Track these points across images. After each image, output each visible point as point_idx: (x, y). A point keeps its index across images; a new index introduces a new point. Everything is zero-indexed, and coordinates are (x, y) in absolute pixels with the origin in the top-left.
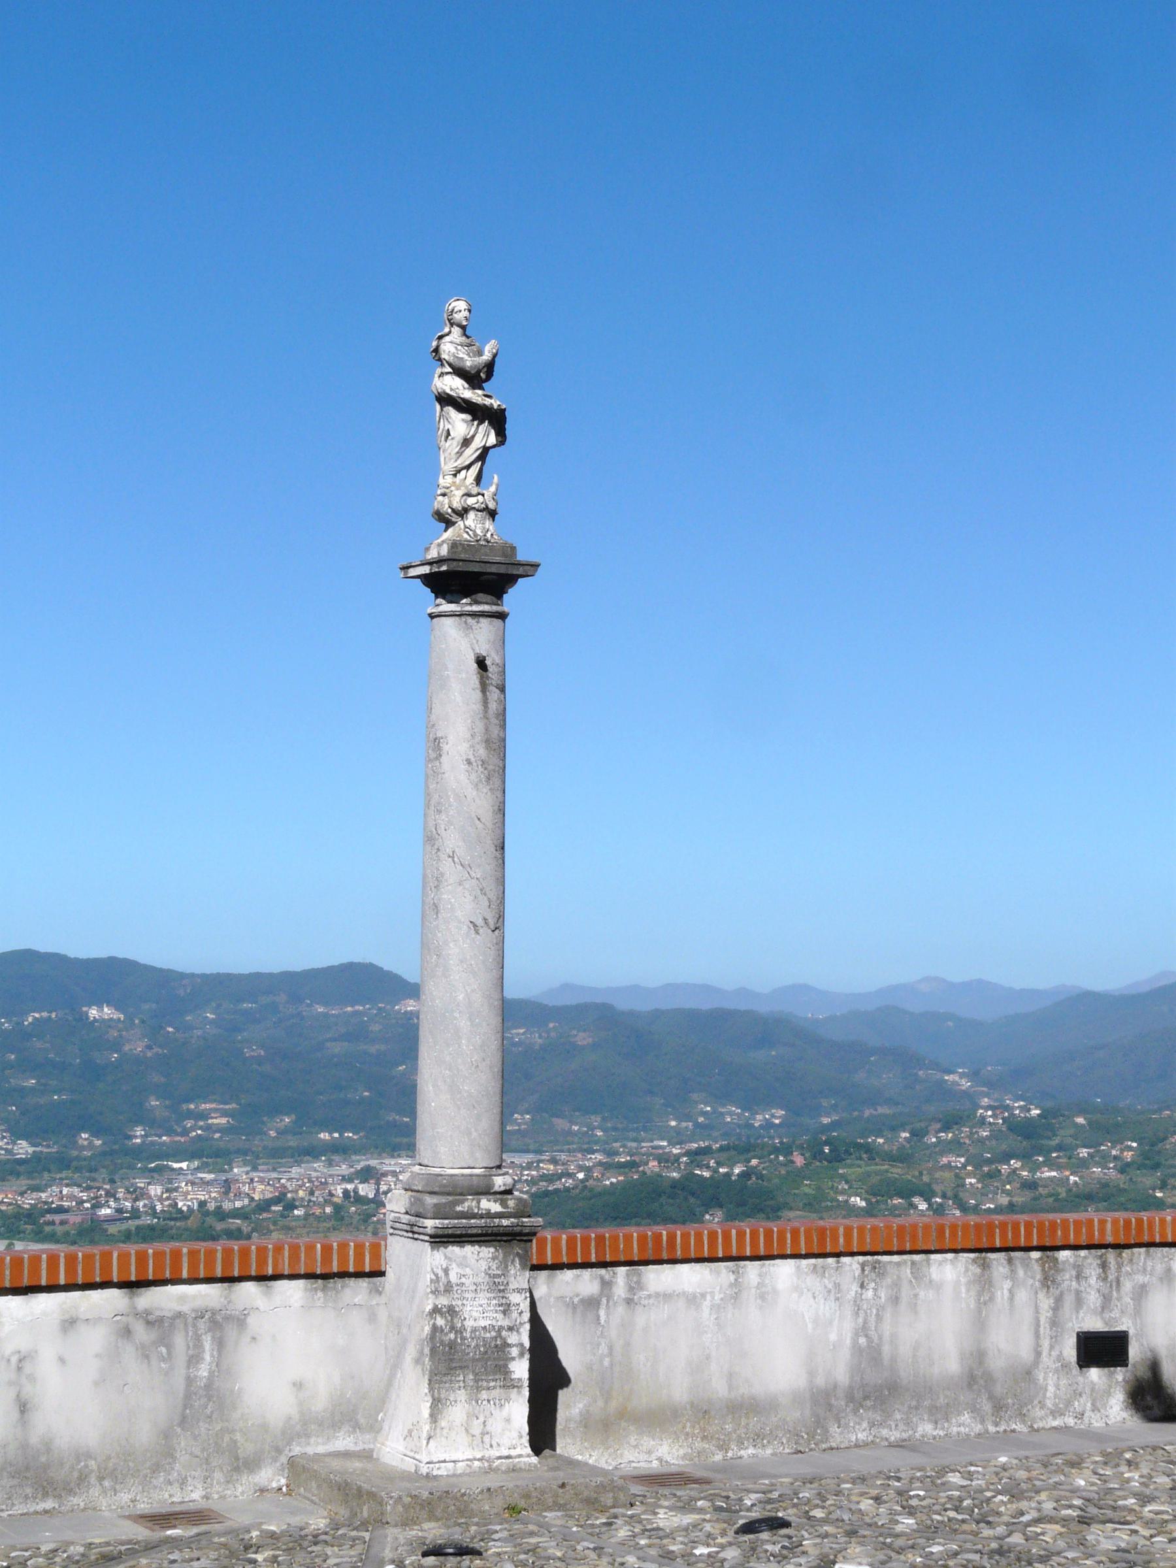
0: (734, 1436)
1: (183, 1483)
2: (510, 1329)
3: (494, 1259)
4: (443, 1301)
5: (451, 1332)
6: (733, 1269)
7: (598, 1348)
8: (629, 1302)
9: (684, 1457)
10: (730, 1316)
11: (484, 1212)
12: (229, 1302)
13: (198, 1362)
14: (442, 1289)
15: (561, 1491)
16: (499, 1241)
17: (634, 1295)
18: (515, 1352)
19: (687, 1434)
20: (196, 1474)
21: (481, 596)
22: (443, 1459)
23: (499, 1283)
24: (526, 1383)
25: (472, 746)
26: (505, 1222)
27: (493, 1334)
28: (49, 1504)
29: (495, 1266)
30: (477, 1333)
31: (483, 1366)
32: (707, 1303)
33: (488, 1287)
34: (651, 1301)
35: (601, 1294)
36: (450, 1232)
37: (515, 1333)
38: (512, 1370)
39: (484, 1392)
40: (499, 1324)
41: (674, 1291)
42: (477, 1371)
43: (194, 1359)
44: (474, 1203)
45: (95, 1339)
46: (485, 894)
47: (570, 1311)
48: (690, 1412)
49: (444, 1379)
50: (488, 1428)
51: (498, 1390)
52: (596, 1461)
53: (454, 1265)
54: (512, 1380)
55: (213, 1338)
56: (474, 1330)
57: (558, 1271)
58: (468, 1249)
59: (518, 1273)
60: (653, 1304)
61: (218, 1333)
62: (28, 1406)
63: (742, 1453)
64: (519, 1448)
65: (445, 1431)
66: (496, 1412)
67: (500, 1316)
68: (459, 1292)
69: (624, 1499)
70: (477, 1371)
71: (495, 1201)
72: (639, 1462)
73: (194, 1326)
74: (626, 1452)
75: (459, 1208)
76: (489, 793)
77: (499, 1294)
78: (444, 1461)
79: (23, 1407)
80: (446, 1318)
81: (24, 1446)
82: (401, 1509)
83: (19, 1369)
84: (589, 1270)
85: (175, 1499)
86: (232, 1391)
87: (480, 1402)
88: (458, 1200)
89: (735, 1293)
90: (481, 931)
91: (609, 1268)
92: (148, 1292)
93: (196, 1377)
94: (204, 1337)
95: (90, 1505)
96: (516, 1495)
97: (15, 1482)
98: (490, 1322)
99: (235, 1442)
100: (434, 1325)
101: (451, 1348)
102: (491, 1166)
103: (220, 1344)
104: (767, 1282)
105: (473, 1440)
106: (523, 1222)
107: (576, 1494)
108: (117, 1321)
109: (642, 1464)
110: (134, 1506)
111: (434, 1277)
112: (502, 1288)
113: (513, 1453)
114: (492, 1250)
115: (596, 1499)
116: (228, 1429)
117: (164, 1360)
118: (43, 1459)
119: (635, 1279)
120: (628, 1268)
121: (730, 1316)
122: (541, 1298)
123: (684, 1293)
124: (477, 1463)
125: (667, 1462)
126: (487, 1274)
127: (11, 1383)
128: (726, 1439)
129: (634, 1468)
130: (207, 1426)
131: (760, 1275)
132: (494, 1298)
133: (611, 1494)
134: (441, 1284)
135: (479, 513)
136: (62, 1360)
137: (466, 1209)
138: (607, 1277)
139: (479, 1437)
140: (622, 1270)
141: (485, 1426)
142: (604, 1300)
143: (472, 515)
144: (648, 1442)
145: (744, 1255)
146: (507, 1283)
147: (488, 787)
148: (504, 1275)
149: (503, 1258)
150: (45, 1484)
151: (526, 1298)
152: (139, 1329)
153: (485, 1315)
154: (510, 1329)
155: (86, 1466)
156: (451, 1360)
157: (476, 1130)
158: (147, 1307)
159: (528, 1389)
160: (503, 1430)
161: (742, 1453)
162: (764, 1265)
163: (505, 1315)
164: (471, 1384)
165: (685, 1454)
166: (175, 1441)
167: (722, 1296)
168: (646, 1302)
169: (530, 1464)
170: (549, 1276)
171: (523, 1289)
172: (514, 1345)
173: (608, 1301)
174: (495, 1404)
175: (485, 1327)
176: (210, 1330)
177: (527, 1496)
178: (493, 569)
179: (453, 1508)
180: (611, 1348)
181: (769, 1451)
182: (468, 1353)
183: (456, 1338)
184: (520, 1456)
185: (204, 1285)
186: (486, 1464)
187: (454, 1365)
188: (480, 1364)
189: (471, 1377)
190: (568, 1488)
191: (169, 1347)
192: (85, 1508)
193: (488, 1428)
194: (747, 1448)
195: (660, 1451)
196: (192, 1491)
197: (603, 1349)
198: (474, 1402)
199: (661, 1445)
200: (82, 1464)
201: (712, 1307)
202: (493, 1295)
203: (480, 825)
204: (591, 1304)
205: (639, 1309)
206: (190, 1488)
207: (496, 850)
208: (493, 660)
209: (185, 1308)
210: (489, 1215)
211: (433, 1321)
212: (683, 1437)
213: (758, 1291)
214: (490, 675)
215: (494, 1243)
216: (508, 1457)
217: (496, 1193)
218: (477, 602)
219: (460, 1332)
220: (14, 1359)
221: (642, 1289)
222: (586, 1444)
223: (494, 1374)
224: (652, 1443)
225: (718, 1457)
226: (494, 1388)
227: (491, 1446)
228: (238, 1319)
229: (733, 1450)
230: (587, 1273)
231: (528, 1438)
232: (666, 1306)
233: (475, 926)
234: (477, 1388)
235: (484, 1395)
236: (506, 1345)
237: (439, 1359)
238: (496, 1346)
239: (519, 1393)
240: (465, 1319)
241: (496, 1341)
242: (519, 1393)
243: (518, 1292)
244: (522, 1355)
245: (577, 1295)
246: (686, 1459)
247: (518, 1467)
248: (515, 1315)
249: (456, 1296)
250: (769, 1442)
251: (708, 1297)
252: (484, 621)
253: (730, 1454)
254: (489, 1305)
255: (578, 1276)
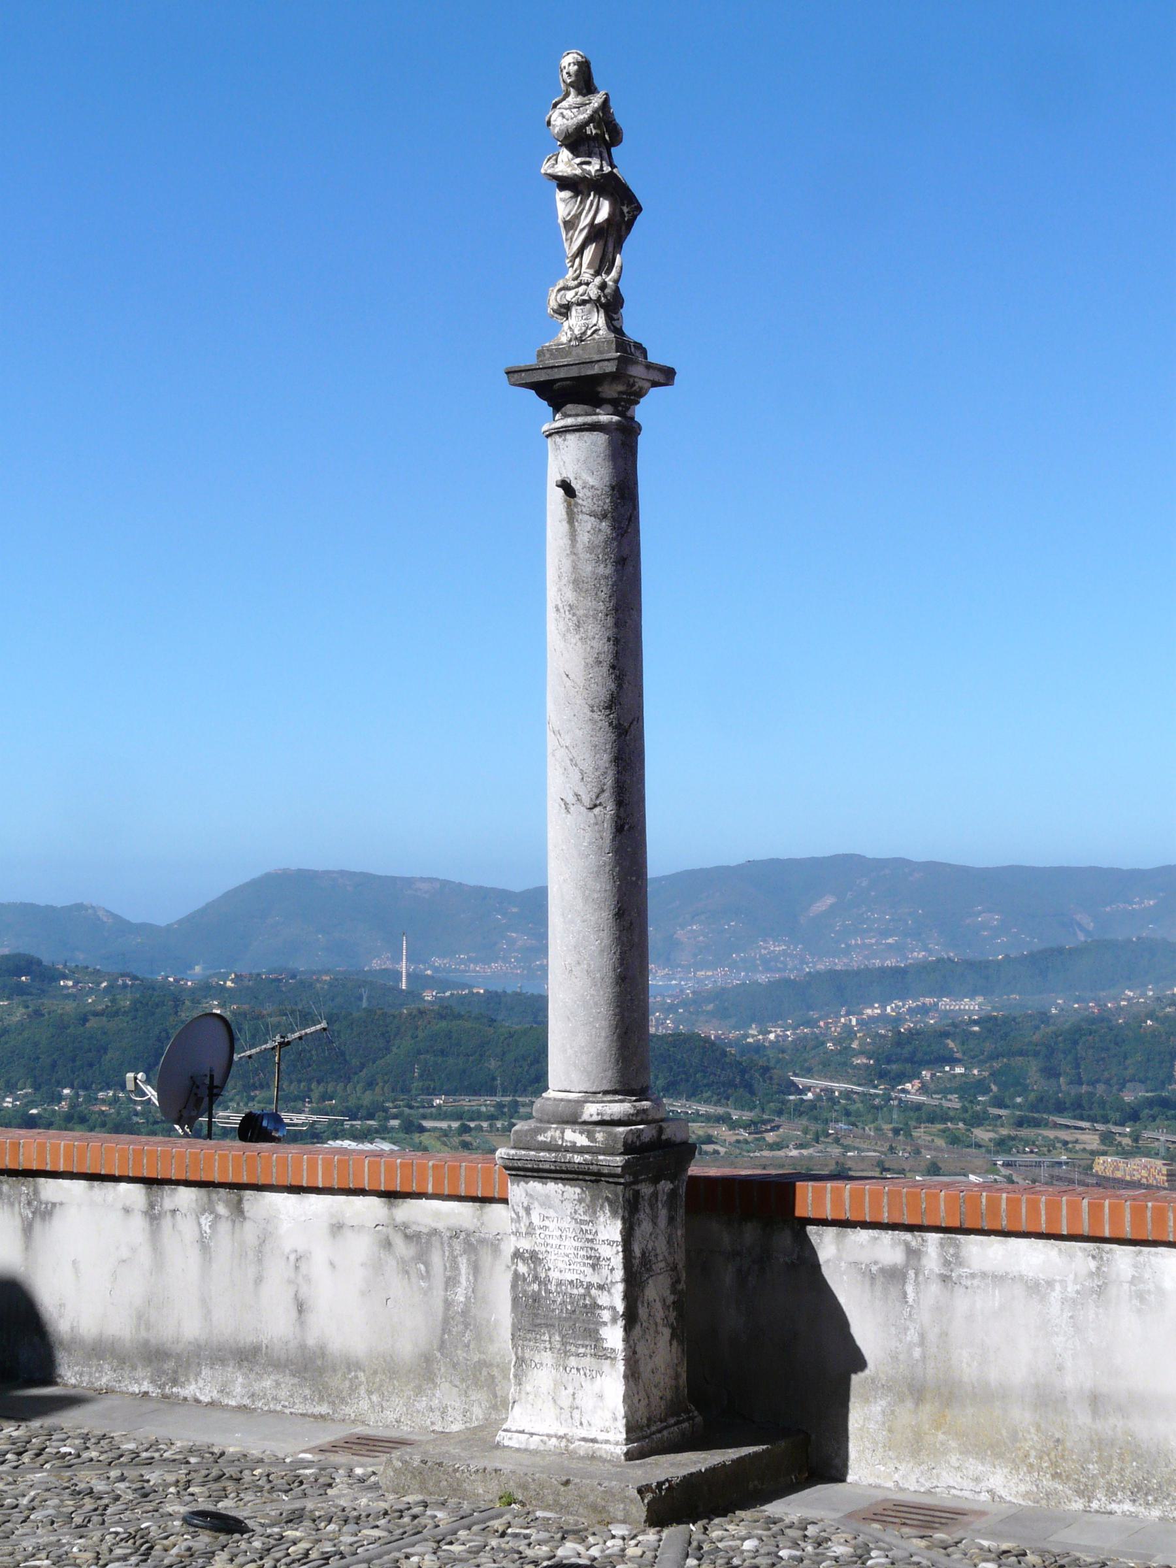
0: (1102, 1482)
1: (443, 1413)
2: (601, 1287)
3: (580, 1201)
4: (525, 1244)
5: (534, 1282)
6: (1094, 1253)
7: (906, 1334)
8: (945, 1279)
9: (1027, 1495)
10: (1091, 1315)
11: (569, 1144)
12: (482, 1224)
13: (454, 1286)
14: (523, 1230)
15: (563, 1488)
16: (585, 1180)
17: (951, 1271)
18: (606, 1315)
19: (1031, 1465)
20: (457, 1405)
21: (569, 408)
22: (521, 1429)
23: (586, 1230)
24: (621, 1355)
25: (560, 590)
26: (578, 1159)
27: (582, 1291)
28: (324, 1409)
29: (582, 1210)
30: (563, 1287)
31: (570, 1327)
32: (1056, 1294)
33: (574, 1234)
34: (976, 1282)
35: (907, 1265)
36: (520, 1164)
37: (606, 1293)
38: (603, 1336)
39: (572, 1358)
40: (588, 1279)
41: (1007, 1273)
42: (564, 1332)
43: (451, 1282)
44: (558, 1134)
45: (360, 1247)
46: (576, 765)
47: (867, 1280)
48: (1036, 1438)
49: (529, 1336)
50: (578, 1402)
51: (588, 1359)
52: (904, 1477)
53: (536, 1204)
54: (605, 1349)
55: (468, 1260)
56: (560, 1283)
57: (849, 1230)
58: (551, 1186)
59: (608, 1222)
60: (979, 1287)
61: (473, 1256)
62: (305, 1307)
63: (1114, 1507)
64: (613, 1432)
65: (531, 1397)
66: (587, 1384)
67: (589, 1270)
68: (542, 1236)
69: (637, 1515)
70: (564, 1332)
71: (581, 1133)
72: (961, 1490)
73: (450, 1246)
74: (944, 1474)
75: (541, 1138)
76: (579, 644)
77: (587, 1245)
78: (522, 1432)
79: (301, 1308)
80: (528, 1264)
81: (303, 1347)
82: (392, 1474)
83: (297, 1268)
84: (890, 1232)
85: (436, 1428)
86: (488, 1321)
87: (568, 1369)
88: (541, 1128)
89: (1098, 1286)
90: (572, 809)
91: (916, 1233)
92: (405, 1204)
93: (453, 1300)
94: (459, 1259)
95: (360, 1418)
96: (511, 1483)
97: (296, 1380)
98: (577, 1276)
99: (493, 1377)
100: (516, 1270)
101: (535, 1301)
102: (593, 1090)
103: (476, 1269)
104: (1147, 1276)
105: (561, 1414)
106: (598, 1160)
107: (580, 1497)
108: (379, 1231)
109: (967, 1494)
110: (398, 1427)
111: (514, 1216)
112: (590, 1237)
113: (601, 1436)
114: (578, 1190)
115: (604, 1507)
116: (485, 1361)
117: (422, 1278)
118: (319, 1363)
119: (952, 1251)
120: (941, 1235)
121: (1091, 1315)
122: (828, 1261)
123: (1021, 1277)
124: (554, 1441)
125: (1001, 1497)
126: (573, 1218)
127: (290, 1282)
128: (1090, 1483)
129: (954, 1496)
130: (465, 1355)
131: (1135, 1266)
132: (582, 1248)
133: (622, 1506)
134: (522, 1225)
135: (579, 308)
136: (332, 1265)
137: (549, 1140)
138: (914, 1244)
139: (568, 1410)
140: (933, 1238)
141: (574, 1399)
142: (911, 1273)
143: (575, 312)
144: (974, 1466)
145: (1102, 1235)
146: (596, 1232)
147: (578, 637)
148: (592, 1221)
149: (591, 1201)
150: (321, 1388)
151: (618, 1252)
152: (398, 1241)
153: (572, 1267)
154: (601, 1287)
155: (356, 1377)
156: (536, 1315)
157: (572, 1047)
158: (404, 1220)
159: (622, 1362)
160: (595, 1407)
161: (1114, 1507)
162: (1140, 1252)
163: (594, 1269)
164: (558, 1346)
165: (1027, 1492)
166: (435, 1366)
167: (1078, 1287)
168: (969, 1283)
169: (612, 1453)
170: (838, 1234)
171: (614, 1242)
172: (605, 1308)
173: (916, 1274)
174: (585, 1374)
175: (572, 1281)
176: (465, 1252)
177: (524, 1487)
178: (562, 374)
179: (445, 1483)
180: (922, 1337)
181: (1156, 1513)
182: (554, 1310)
183: (540, 1290)
184: (607, 1442)
185: (456, 1203)
186: (563, 1444)
187: (539, 1321)
188: (567, 1325)
189: (558, 1338)
190: (571, 1486)
191: (427, 1265)
192: (355, 1420)
193: (578, 1402)
194: (1120, 1502)
195: (991, 1480)
196: (452, 1422)
197: (912, 1336)
198: (561, 1368)
199: (994, 1473)
200: (353, 1374)
201: (1064, 1301)
202: (580, 1245)
203: (569, 683)
204: (894, 1276)
205: (959, 1290)
206: (450, 1419)
207: (593, 711)
208: (584, 483)
209: (440, 1226)
210: (575, 1149)
211: (514, 1267)
212: (1025, 1469)
213: (1133, 1288)
214: (580, 501)
215: (581, 1182)
216: (594, 1441)
217: (585, 1123)
218: (566, 416)
219: (544, 1283)
220: (292, 1257)
221: (961, 1264)
222: (890, 1453)
223: (585, 1338)
224: (980, 1468)
225: (1078, 1505)
226: (585, 1355)
227: (581, 1424)
228: (492, 1244)
229: (1099, 1500)
230: (887, 1237)
231: (624, 1421)
232: (997, 1292)
233: (566, 804)
234: (565, 1352)
235: (573, 1362)
236: (595, 1306)
237: (523, 1312)
238: (585, 1306)
239: (613, 1365)
240: (549, 1269)
241: (585, 1299)
242: (613, 1365)
243: (609, 1244)
244: (614, 1320)
245: (876, 1263)
246: (1030, 1499)
247: (598, 1454)
248: (605, 1271)
249: (539, 1240)
250: (1156, 1500)
251: (1058, 1287)
252: (572, 438)
253: (1095, 1505)
254: (576, 1256)
255: (876, 1239)
